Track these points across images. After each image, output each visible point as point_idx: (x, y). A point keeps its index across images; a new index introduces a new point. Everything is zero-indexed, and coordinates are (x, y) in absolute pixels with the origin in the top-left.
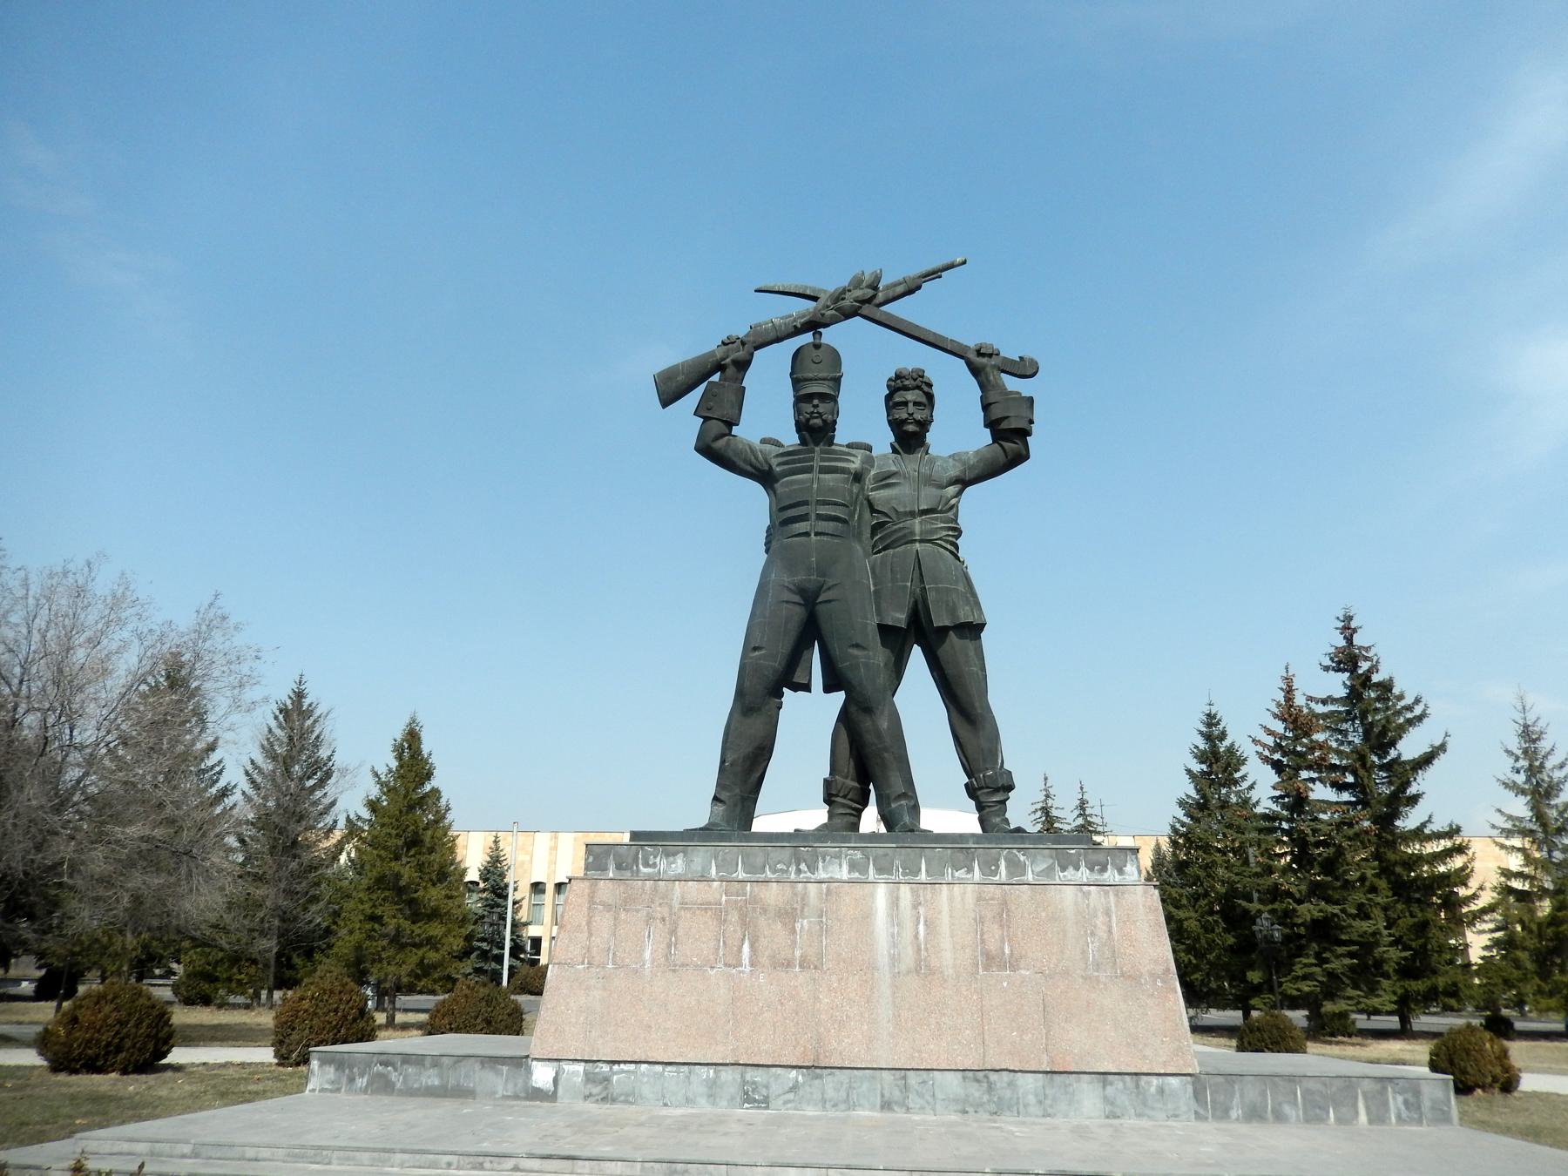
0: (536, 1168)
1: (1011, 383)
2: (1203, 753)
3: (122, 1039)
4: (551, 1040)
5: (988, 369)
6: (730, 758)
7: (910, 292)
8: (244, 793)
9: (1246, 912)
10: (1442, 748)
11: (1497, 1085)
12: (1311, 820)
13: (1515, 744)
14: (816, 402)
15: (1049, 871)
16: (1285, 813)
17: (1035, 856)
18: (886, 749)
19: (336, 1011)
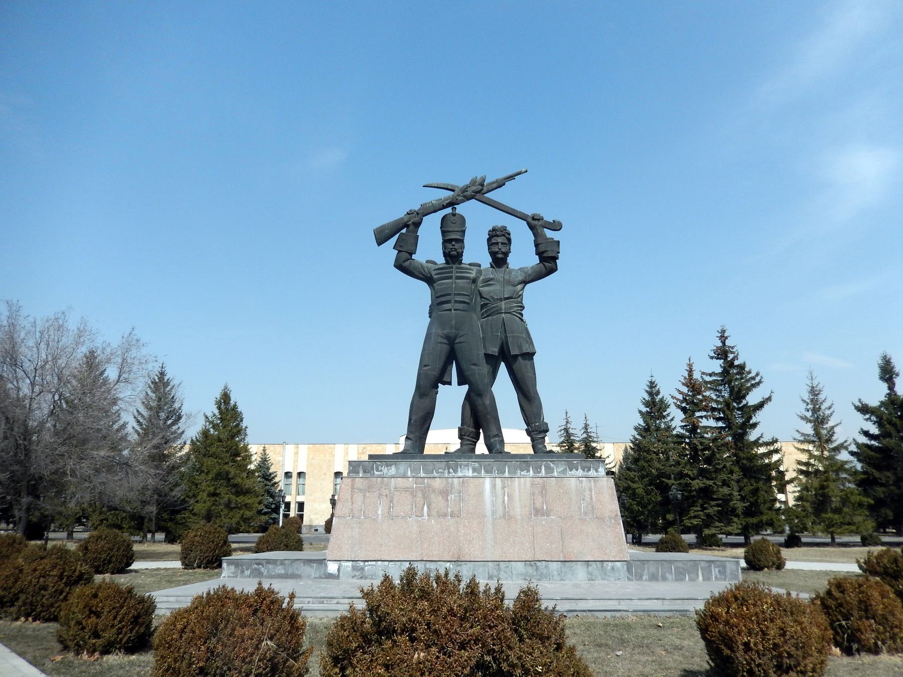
1: (549, 234)
3: (111, 557)
4: (336, 552)
5: (538, 227)
6: (414, 418)
7: (500, 186)
8: (133, 428)
9: (667, 484)
10: (769, 399)
11: (775, 566)
12: (700, 438)
13: (807, 396)
14: (453, 243)
15: (564, 471)
16: (687, 434)
18: (488, 413)
19: (213, 542)
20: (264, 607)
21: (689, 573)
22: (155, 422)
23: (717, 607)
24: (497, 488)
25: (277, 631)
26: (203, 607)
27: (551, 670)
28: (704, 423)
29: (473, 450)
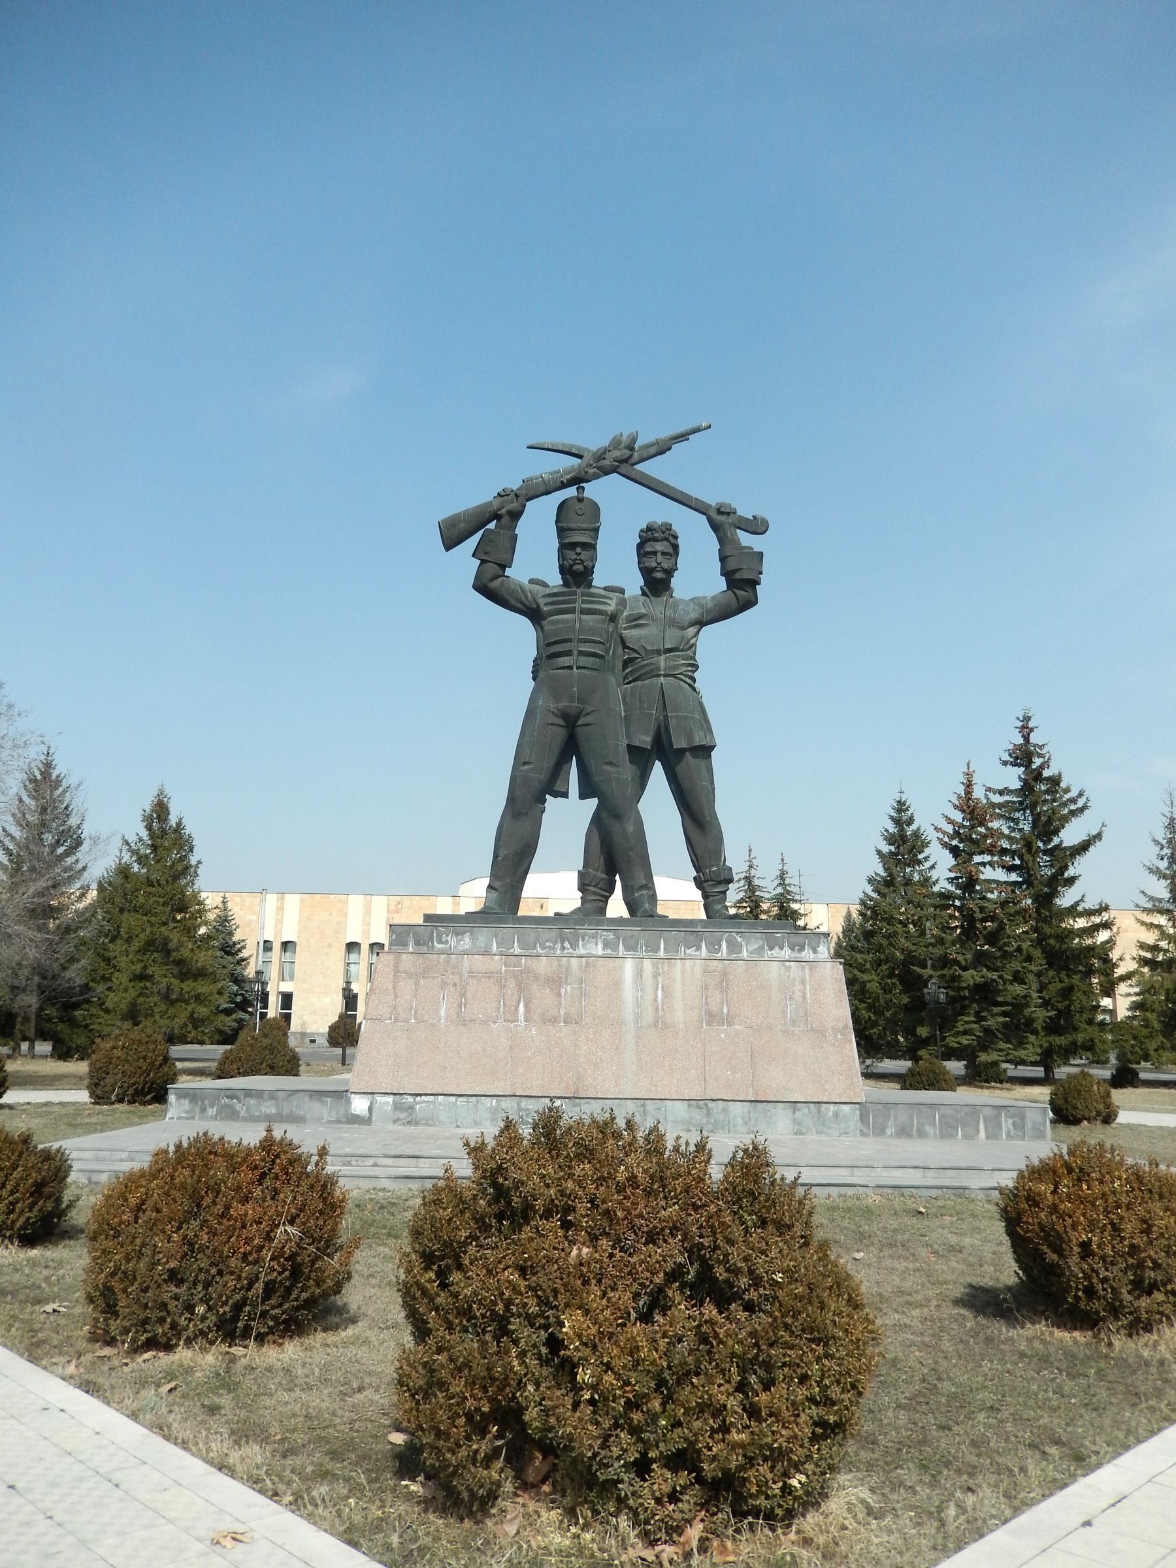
0: (390, 1164)
1: (745, 539)
2: (892, 836)
5: (726, 526)
6: (503, 853)
9: (920, 976)
10: (1098, 837)
14: (578, 550)
16: (958, 892)
17: (750, 938)
19: (145, 1058)
20: (276, 1170)
21: (964, 1125)
22: (35, 849)
23: (1038, 1183)
24: (645, 975)
25: (301, 1210)
26: (173, 1169)
27: (797, 1280)
28: (988, 873)
29: (603, 911)
